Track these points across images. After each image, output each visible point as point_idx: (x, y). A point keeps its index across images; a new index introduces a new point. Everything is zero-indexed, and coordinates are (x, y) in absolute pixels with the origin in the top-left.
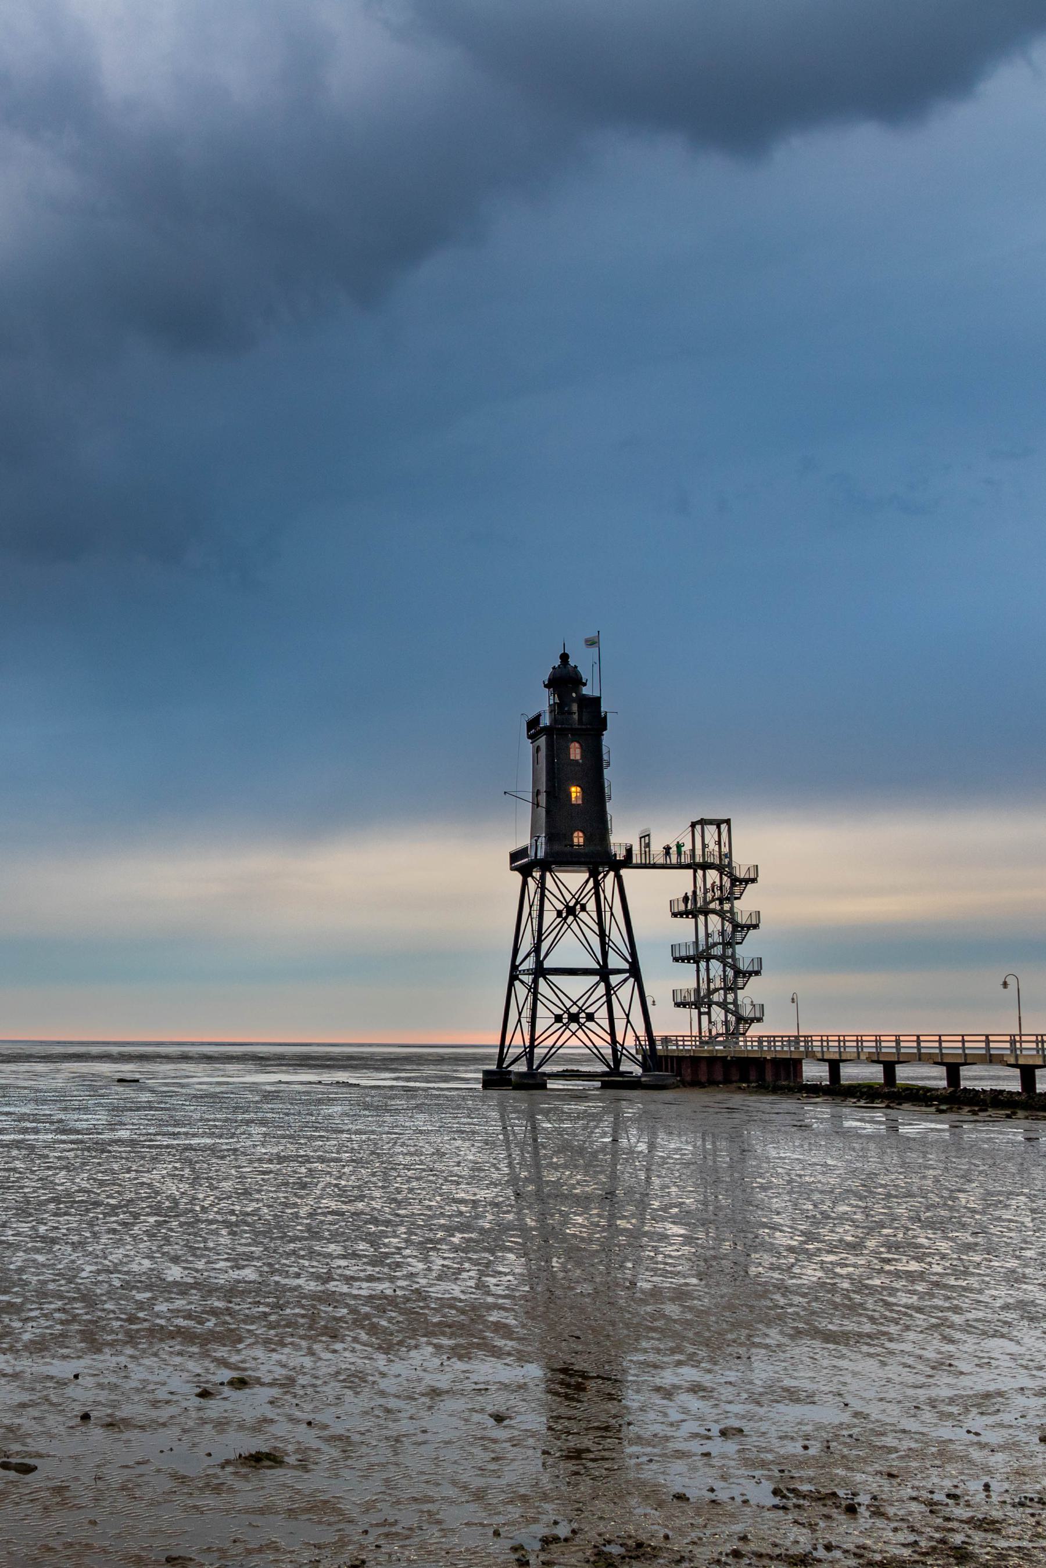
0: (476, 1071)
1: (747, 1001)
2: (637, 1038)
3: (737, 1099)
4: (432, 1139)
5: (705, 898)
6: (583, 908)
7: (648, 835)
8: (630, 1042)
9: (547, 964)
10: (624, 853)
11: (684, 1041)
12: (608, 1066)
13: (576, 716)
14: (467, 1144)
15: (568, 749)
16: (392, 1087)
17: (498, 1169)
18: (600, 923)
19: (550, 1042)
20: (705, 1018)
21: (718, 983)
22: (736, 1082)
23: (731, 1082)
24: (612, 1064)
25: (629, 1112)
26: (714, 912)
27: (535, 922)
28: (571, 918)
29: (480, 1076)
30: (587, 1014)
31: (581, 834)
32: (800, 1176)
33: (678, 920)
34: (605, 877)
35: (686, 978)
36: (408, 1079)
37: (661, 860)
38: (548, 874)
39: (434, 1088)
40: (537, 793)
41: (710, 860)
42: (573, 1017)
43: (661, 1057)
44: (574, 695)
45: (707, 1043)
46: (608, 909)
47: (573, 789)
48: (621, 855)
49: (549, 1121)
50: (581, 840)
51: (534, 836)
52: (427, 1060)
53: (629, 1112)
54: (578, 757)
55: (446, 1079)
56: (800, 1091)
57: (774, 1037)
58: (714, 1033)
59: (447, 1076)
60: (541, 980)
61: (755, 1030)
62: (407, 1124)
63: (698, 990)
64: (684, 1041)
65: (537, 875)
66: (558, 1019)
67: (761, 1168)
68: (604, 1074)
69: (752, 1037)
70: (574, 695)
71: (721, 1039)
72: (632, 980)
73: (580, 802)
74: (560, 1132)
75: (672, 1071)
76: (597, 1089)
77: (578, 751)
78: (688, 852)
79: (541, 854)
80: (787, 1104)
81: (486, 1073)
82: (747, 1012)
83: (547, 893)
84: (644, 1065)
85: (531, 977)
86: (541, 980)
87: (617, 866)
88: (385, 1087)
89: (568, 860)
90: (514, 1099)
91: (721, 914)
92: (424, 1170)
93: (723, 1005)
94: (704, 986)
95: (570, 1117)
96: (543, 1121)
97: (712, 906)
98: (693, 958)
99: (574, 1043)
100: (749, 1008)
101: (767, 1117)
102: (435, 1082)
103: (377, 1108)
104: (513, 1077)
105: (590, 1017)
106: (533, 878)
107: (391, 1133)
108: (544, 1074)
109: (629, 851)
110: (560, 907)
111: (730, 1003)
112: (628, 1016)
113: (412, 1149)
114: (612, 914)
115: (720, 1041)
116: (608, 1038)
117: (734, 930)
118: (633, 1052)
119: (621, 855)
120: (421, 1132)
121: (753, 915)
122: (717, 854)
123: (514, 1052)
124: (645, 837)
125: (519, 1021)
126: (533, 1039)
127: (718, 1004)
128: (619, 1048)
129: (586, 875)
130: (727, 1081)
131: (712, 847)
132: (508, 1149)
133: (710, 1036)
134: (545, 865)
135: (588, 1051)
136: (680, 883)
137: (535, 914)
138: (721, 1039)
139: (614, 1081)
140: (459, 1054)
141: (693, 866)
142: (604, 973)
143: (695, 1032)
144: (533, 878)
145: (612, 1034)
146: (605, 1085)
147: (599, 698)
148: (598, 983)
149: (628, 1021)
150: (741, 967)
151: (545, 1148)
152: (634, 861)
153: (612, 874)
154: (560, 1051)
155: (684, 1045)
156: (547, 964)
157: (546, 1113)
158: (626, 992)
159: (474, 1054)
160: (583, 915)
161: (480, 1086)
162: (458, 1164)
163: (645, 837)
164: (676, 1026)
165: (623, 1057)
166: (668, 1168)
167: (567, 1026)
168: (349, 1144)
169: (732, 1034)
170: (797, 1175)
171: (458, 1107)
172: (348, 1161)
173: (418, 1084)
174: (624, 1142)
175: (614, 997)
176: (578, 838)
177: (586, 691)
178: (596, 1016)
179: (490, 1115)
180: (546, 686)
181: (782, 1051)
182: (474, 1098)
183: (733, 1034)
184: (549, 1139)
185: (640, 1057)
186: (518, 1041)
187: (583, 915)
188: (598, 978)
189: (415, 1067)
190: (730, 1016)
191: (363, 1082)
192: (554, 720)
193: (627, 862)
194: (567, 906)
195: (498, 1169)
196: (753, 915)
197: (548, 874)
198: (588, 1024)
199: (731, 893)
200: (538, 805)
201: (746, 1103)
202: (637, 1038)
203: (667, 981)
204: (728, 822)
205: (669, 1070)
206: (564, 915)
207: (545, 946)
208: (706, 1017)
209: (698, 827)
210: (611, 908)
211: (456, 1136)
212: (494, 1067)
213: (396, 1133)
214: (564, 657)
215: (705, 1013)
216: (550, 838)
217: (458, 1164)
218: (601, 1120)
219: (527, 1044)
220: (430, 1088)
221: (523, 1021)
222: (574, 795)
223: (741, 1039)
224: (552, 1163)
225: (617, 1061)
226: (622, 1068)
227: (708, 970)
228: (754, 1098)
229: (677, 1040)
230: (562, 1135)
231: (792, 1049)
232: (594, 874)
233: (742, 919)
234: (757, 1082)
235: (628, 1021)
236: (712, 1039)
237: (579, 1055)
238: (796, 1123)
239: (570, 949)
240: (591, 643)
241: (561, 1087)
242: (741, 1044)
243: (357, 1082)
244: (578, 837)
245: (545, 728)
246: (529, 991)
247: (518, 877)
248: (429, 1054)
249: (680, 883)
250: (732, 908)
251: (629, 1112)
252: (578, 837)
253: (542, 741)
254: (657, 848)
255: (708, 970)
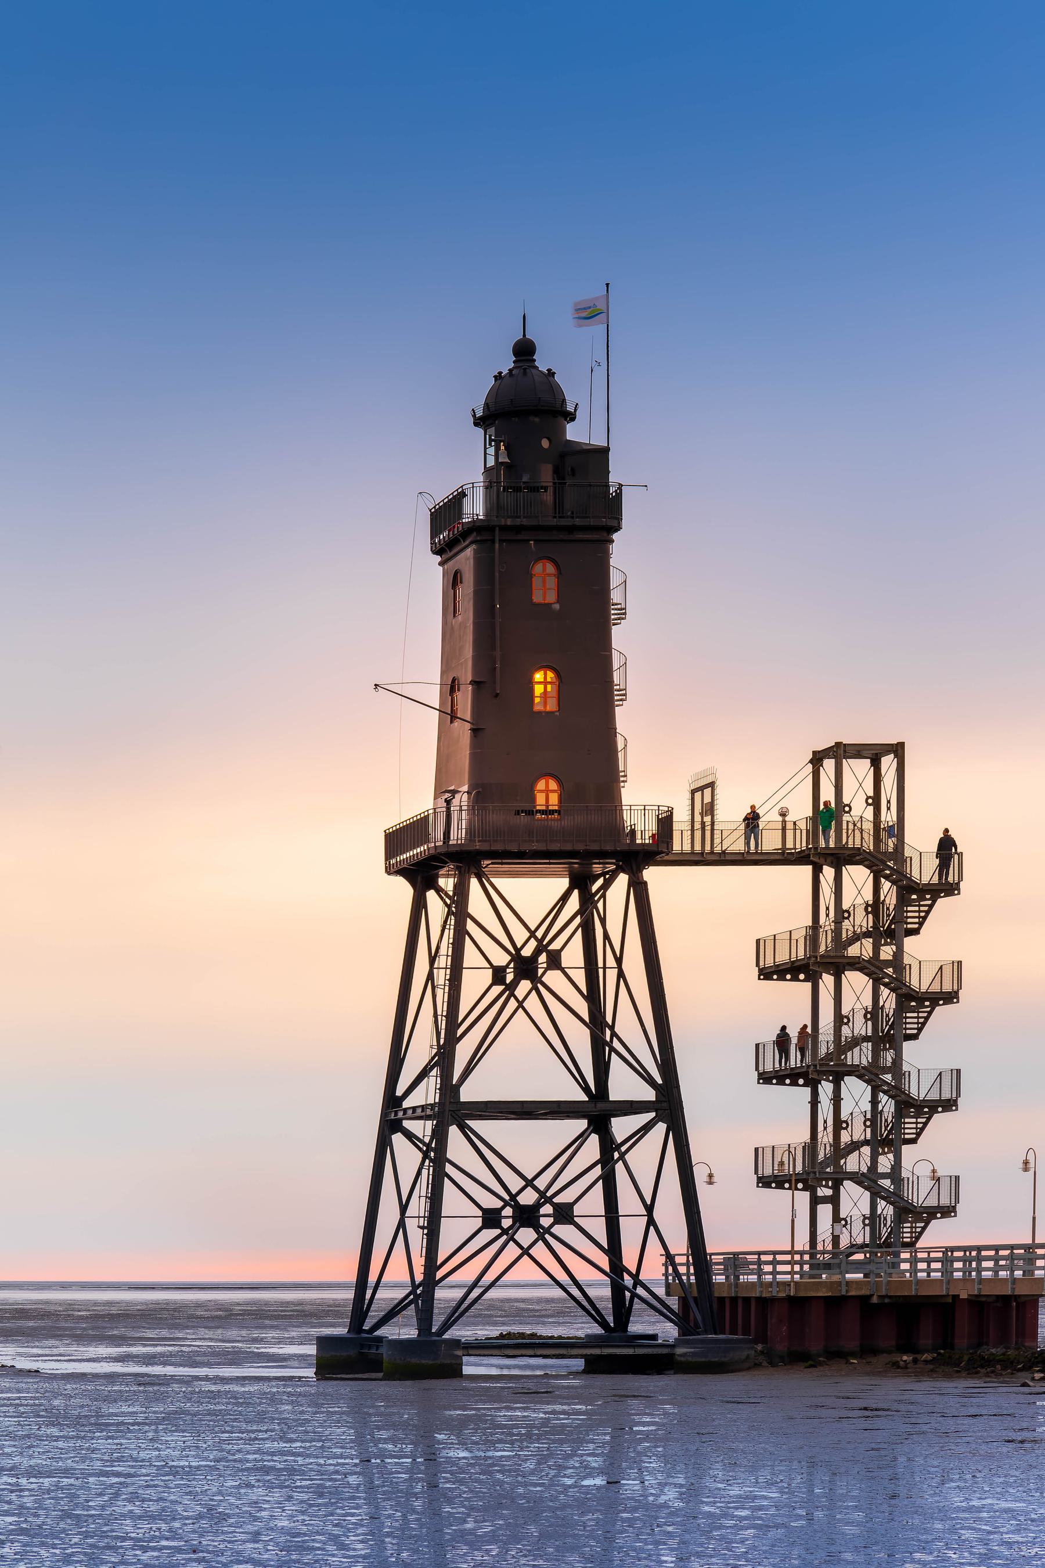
0: (302, 1341)
1: (924, 1171)
2: (670, 1258)
3: (888, 1390)
4: (199, 1486)
5: (837, 931)
6: (555, 961)
7: (712, 785)
8: (654, 1271)
9: (468, 1094)
10: (652, 827)
11: (774, 1263)
12: (603, 1324)
13: (548, 497)
14: (277, 1495)
15: (528, 576)
16: (111, 1377)
17: (343, 1547)
18: (593, 995)
19: (468, 1274)
20: (825, 1211)
21: (859, 1131)
22: (890, 1352)
23: (875, 1352)
24: (610, 1319)
25: (645, 1423)
26: (856, 964)
27: (442, 996)
28: (525, 985)
29: (311, 1350)
30: (556, 1206)
31: (553, 785)
32: (1009, 1544)
33: (774, 986)
34: (606, 886)
35: (785, 1119)
36: (149, 1360)
37: (736, 844)
38: (474, 882)
39: (206, 1378)
40: (451, 687)
41: (853, 841)
42: (523, 1216)
43: (721, 1300)
44: (545, 444)
45: (827, 1266)
46: (611, 962)
47: (538, 676)
48: (645, 829)
49: (463, 1444)
50: (554, 799)
51: (444, 790)
52: (191, 1317)
53: (645, 1423)
54: (551, 597)
55: (235, 1358)
56: (1028, 1368)
57: (979, 1249)
58: (844, 1242)
59: (237, 1352)
60: (454, 1131)
61: (938, 1235)
62: (143, 1455)
63: (811, 1147)
64: (774, 1263)
65: (448, 883)
66: (491, 1219)
67: (926, 1531)
68: (591, 1341)
69: (929, 1250)
70: (545, 444)
71: (859, 1256)
72: (661, 1127)
73: (552, 706)
74: (487, 1467)
75: (746, 1331)
76: (576, 1374)
77: (552, 582)
78: (802, 825)
79: (458, 835)
80: (999, 1396)
81: (323, 1342)
82: (921, 1195)
83: (470, 926)
84: (682, 1319)
85: (429, 1125)
86: (454, 1131)
87: (635, 859)
88: (96, 1376)
89: (527, 854)
90: (386, 1398)
91: (872, 968)
92: (178, 1550)
93: (868, 1180)
94: (826, 1138)
95: (510, 1434)
96: (448, 1446)
97: (853, 951)
98: (804, 1075)
99: (525, 1277)
100: (926, 1184)
101: (950, 1424)
102: (209, 1365)
103: (78, 1422)
104: (384, 1350)
105: (564, 1214)
106: (439, 890)
107: (107, 1474)
108: (456, 1343)
109: (666, 823)
110: (501, 959)
111: (884, 1176)
112: (650, 1209)
113: (154, 1507)
114: (621, 975)
115: (858, 1263)
116: (604, 1261)
117: (901, 1007)
118: (660, 1291)
119: (645, 829)
120: (174, 1472)
121: (947, 971)
122: (868, 826)
123: (387, 1296)
124: (704, 793)
125: (402, 1225)
126: (431, 1264)
127: (857, 1178)
128: (628, 1281)
129: (564, 883)
130: (868, 1351)
131: (860, 810)
132: (371, 1500)
133: (835, 1254)
134: (469, 861)
135: (559, 1293)
136: (780, 901)
137: (441, 977)
138: (859, 1256)
139: (615, 1354)
140: (267, 1303)
141: (812, 858)
142: (597, 1111)
143: (802, 1242)
144: (439, 890)
145: (614, 1249)
146: (595, 1366)
147: (605, 451)
148: (583, 1137)
149: (651, 1222)
150: (914, 1092)
151: (450, 1501)
152: (676, 847)
153: (623, 879)
154: (492, 1294)
155: (774, 1273)
156: (468, 1094)
157: (457, 1427)
158: (646, 1155)
159: (300, 1303)
160: (553, 978)
161: (310, 1373)
162: (255, 1537)
163: (704, 793)
164: (758, 1228)
165: (637, 1305)
166: (722, 1538)
167: (509, 1235)
168: (13, 1497)
169: (885, 1244)
170: (1003, 1543)
171: (261, 1418)
172: (11, 1532)
173: (170, 1370)
174: (630, 1485)
175: (619, 1167)
176: (547, 794)
177: (574, 432)
178: (577, 1210)
179: (334, 1432)
180: (478, 422)
181: (996, 1280)
182: (294, 1399)
183: (887, 1244)
184: (461, 1482)
185: (673, 1302)
186: (396, 1277)
187: (553, 978)
188: (582, 1124)
189: (165, 1333)
190: (882, 1204)
191: (47, 1367)
192: (493, 505)
193: (659, 850)
194: (517, 957)
195: (343, 1547)
196: (947, 971)
197: (474, 882)
198: (557, 1230)
199: (899, 917)
200: (453, 717)
201: (907, 1396)
202: (670, 1258)
203: (741, 1122)
204: (898, 750)
205: (739, 1329)
206: (510, 978)
207: (463, 1052)
208: (829, 1207)
209: (829, 764)
210: (619, 960)
211: (252, 1479)
212: (342, 1331)
213: (118, 1475)
214: (524, 351)
215: (825, 1200)
216: (481, 795)
217: (255, 1537)
218: (581, 1442)
219: (419, 1278)
220: (197, 1378)
221: (411, 1225)
222: (539, 689)
223: (905, 1255)
224: (463, 1533)
225: (622, 1310)
226: (635, 1327)
227: (837, 1100)
228: (927, 1385)
229: (759, 1263)
230: (491, 1473)
231: (1018, 1273)
232: (580, 882)
233: (921, 980)
234: (935, 1349)
235: (651, 1222)
236: (840, 1257)
237: (539, 1301)
238: (1012, 1435)
239: (523, 1058)
240: (590, 313)
241: (494, 1372)
242: (905, 1266)
243: (34, 1366)
244: (547, 791)
245: (476, 528)
246: (426, 1155)
247: (403, 890)
248: (199, 1305)
249: (780, 901)
250: (899, 954)
251: (645, 1423)
252: (547, 791)
253: (466, 558)
254: (730, 813)
255: (837, 1100)
